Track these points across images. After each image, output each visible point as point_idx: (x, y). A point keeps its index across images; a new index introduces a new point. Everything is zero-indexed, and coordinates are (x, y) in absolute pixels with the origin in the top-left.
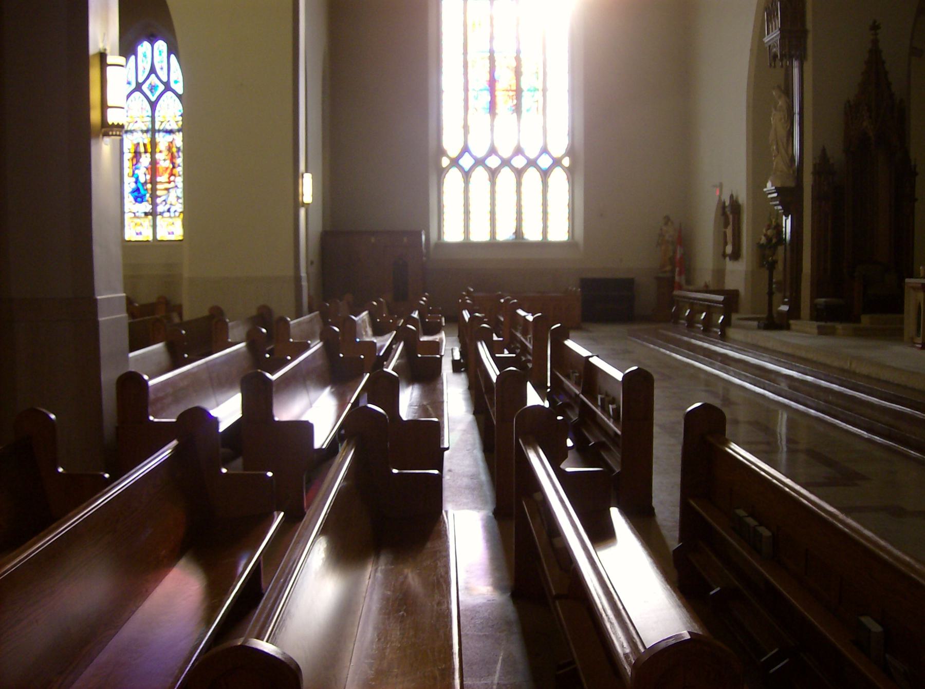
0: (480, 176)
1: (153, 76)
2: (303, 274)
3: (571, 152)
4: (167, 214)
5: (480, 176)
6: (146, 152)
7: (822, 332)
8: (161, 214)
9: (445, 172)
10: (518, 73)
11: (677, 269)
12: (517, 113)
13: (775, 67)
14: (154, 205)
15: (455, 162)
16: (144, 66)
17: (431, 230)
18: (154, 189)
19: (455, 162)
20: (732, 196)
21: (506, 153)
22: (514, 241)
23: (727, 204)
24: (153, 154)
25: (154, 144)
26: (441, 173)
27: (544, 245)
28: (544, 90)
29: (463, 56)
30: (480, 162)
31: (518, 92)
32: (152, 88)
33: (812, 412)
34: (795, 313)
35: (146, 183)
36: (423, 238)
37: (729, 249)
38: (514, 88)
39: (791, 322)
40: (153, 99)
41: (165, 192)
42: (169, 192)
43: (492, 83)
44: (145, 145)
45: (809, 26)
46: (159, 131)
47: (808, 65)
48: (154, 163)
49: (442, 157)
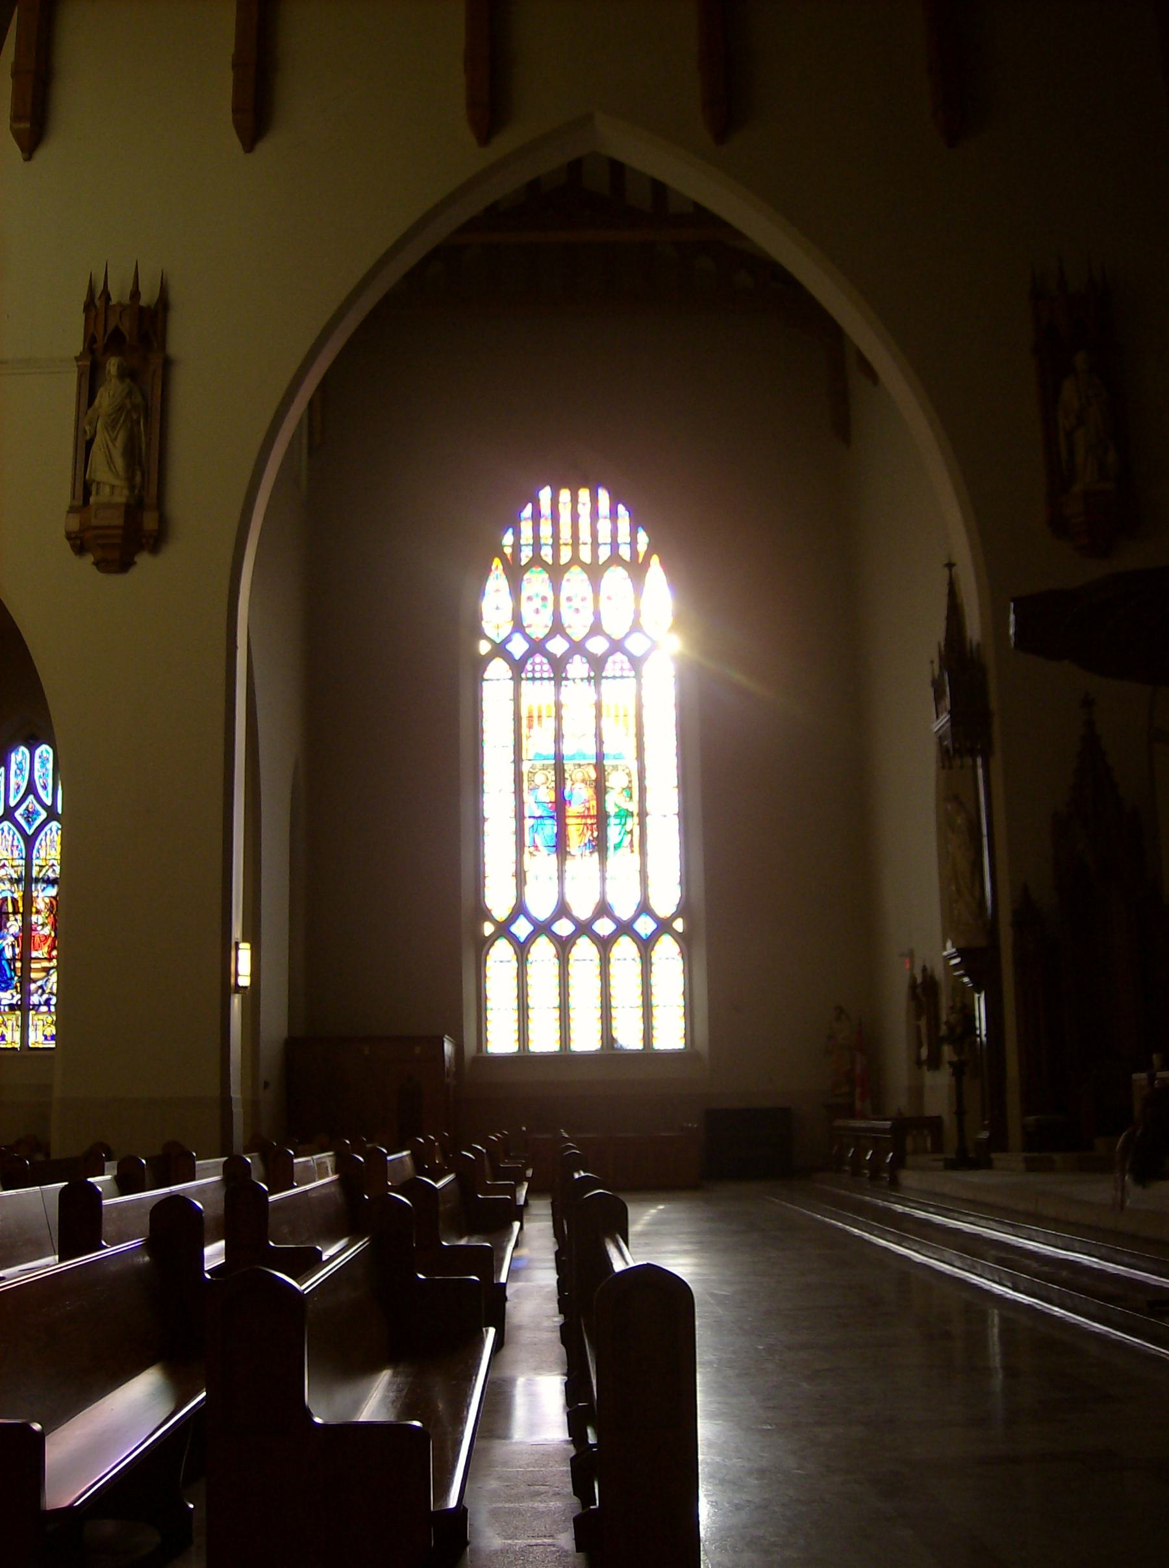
0: (543, 951)
1: (31, 798)
2: (236, 1093)
3: (684, 910)
4: (44, 1009)
5: (543, 951)
6: (15, 912)
7: (1032, 1167)
8: (36, 1007)
9: (489, 944)
10: (600, 788)
11: (858, 1090)
12: (599, 852)
13: (951, 767)
14: (26, 993)
15: (503, 929)
16: (19, 781)
17: (465, 1040)
18: (26, 969)
19: (503, 929)
20: (924, 969)
21: (583, 911)
22: (598, 1053)
23: (919, 980)
24: (26, 915)
25: (28, 899)
26: (483, 945)
27: (648, 1057)
28: (643, 814)
29: (513, 765)
30: (542, 928)
31: (601, 819)
32: (30, 815)
33: (1058, 1311)
34: (998, 1142)
35: (14, 959)
36: (448, 1048)
37: (924, 1052)
38: (593, 812)
39: (993, 1156)
40: (30, 832)
41: (44, 974)
42: (48, 975)
43: (560, 805)
44: (14, 901)
45: (994, 705)
46: (37, 880)
47: (996, 763)
48: (27, 929)
49: (484, 922)
